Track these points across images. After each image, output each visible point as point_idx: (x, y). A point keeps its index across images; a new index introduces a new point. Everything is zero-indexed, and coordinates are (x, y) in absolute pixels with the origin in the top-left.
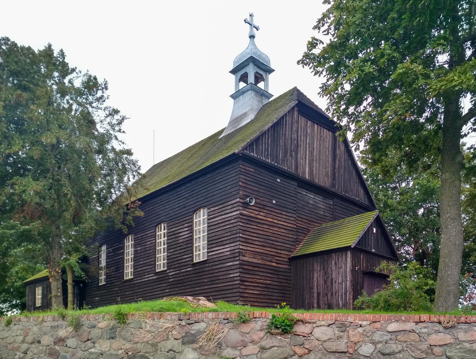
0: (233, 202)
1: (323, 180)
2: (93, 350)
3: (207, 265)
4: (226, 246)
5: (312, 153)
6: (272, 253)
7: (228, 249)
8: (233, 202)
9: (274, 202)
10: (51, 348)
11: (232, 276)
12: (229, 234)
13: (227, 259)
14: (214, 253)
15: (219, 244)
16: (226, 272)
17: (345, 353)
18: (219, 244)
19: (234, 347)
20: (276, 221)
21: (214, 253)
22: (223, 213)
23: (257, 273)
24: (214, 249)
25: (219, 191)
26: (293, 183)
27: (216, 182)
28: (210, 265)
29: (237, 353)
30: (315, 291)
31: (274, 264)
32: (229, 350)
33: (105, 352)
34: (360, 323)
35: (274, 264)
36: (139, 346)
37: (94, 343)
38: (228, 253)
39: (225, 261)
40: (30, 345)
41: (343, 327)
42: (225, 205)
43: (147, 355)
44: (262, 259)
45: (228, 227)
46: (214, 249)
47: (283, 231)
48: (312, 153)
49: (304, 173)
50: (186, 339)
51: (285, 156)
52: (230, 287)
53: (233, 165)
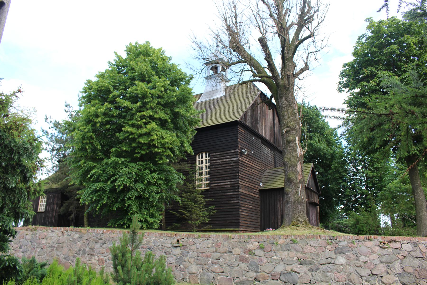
0: (233, 151)
1: (270, 138)
2: (275, 257)
3: (210, 193)
4: (227, 181)
5: (265, 122)
6: (252, 187)
7: (229, 183)
8: (233, 151)
9: (252, 152)
10: (242, 256)
11: (232, 202)
12: (230, 173)
13: (228, 190)
14: (216, 185)
15: (221, 179)
16: (227, 199)
17: (422, 257)
18: (221, 179)
19: (366, 256)
20: (253, 165)
21: (216, 185)
22: (224, 158)
23: (247, 200)
24: (216, 182)
25: (221, 143)
26: (260, 140)
27: (218, 136)
28: (213, 193)
29: (367, 258)
30: (279, 213)
31: (253, 194)
32: (363, 257)
33: (285, 259)
34: (422, 242)
35: (253, 194)
36: (307, 255)
37: (275, 253)
38: (229, 186)
39: (226, 191)
40: (222, 254)
41: (415, 244)
42: (225, 152)
43: (313, 260)
44: (248, 191)
45: (228, 167)
46: (216, 182)
47: (256, 171)
48: (265, 122)
49: (262, 133)
50: (337, 251)
51: (256, 124)
52: (231, 210)
53: (248, 132)
